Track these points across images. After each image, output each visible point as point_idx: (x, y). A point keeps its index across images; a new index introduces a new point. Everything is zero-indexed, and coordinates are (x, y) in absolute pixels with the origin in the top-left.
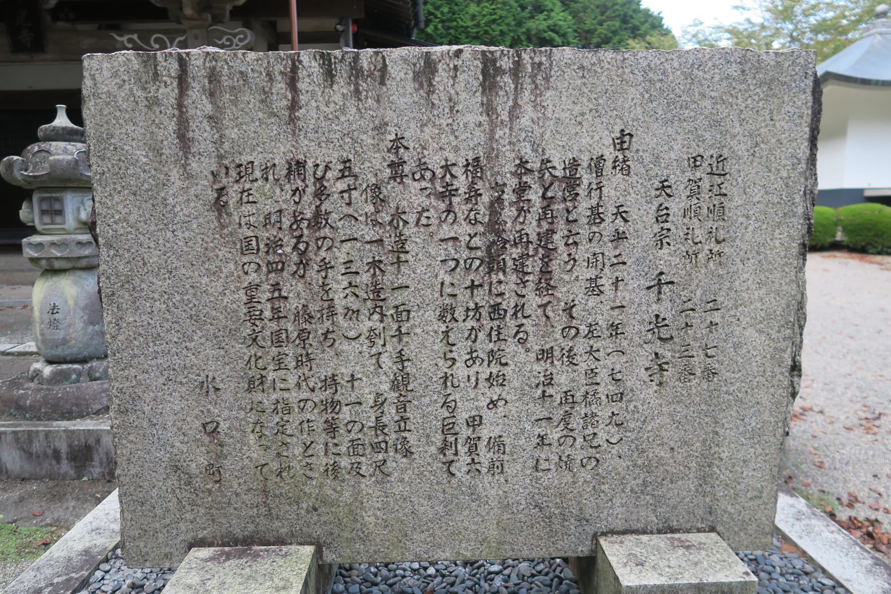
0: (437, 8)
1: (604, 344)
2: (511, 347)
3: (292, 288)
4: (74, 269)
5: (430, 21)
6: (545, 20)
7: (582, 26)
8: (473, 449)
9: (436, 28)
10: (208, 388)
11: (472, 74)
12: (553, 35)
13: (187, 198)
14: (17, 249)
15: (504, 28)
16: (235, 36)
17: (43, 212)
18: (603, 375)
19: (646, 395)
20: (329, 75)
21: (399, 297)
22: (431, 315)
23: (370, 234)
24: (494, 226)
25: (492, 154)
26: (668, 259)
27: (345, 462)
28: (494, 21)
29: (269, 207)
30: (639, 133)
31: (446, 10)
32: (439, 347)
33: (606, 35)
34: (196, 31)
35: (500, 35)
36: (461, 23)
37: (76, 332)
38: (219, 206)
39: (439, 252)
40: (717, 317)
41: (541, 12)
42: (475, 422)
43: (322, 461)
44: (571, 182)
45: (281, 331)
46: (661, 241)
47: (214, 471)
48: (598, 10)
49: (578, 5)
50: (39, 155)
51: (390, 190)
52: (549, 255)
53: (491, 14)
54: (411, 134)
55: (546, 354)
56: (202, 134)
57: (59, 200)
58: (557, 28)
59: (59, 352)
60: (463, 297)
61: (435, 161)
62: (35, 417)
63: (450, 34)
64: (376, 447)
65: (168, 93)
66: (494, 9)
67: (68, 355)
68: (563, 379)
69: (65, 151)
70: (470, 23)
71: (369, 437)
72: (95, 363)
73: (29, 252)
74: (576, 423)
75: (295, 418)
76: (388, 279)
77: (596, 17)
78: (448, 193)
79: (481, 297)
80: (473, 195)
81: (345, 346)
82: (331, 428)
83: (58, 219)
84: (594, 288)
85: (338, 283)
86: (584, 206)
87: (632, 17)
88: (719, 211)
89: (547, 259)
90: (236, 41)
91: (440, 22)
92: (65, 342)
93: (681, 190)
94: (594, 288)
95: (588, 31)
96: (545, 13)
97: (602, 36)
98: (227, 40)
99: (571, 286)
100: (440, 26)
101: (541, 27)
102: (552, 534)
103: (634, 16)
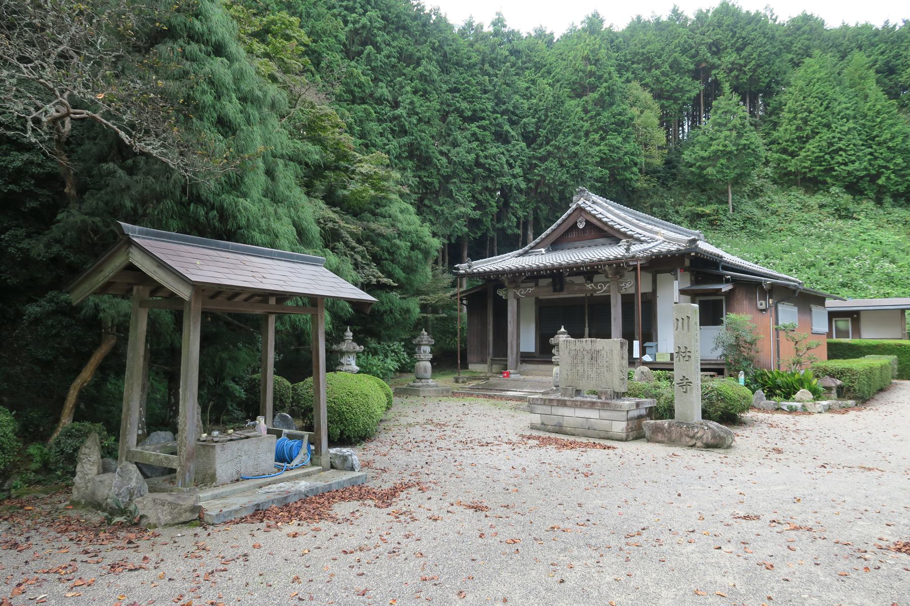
5: (883, 173)
9: (888, 178)
13: (567, 352)
91: (893, 173)
99: (599, 362)
100: (892, 176)
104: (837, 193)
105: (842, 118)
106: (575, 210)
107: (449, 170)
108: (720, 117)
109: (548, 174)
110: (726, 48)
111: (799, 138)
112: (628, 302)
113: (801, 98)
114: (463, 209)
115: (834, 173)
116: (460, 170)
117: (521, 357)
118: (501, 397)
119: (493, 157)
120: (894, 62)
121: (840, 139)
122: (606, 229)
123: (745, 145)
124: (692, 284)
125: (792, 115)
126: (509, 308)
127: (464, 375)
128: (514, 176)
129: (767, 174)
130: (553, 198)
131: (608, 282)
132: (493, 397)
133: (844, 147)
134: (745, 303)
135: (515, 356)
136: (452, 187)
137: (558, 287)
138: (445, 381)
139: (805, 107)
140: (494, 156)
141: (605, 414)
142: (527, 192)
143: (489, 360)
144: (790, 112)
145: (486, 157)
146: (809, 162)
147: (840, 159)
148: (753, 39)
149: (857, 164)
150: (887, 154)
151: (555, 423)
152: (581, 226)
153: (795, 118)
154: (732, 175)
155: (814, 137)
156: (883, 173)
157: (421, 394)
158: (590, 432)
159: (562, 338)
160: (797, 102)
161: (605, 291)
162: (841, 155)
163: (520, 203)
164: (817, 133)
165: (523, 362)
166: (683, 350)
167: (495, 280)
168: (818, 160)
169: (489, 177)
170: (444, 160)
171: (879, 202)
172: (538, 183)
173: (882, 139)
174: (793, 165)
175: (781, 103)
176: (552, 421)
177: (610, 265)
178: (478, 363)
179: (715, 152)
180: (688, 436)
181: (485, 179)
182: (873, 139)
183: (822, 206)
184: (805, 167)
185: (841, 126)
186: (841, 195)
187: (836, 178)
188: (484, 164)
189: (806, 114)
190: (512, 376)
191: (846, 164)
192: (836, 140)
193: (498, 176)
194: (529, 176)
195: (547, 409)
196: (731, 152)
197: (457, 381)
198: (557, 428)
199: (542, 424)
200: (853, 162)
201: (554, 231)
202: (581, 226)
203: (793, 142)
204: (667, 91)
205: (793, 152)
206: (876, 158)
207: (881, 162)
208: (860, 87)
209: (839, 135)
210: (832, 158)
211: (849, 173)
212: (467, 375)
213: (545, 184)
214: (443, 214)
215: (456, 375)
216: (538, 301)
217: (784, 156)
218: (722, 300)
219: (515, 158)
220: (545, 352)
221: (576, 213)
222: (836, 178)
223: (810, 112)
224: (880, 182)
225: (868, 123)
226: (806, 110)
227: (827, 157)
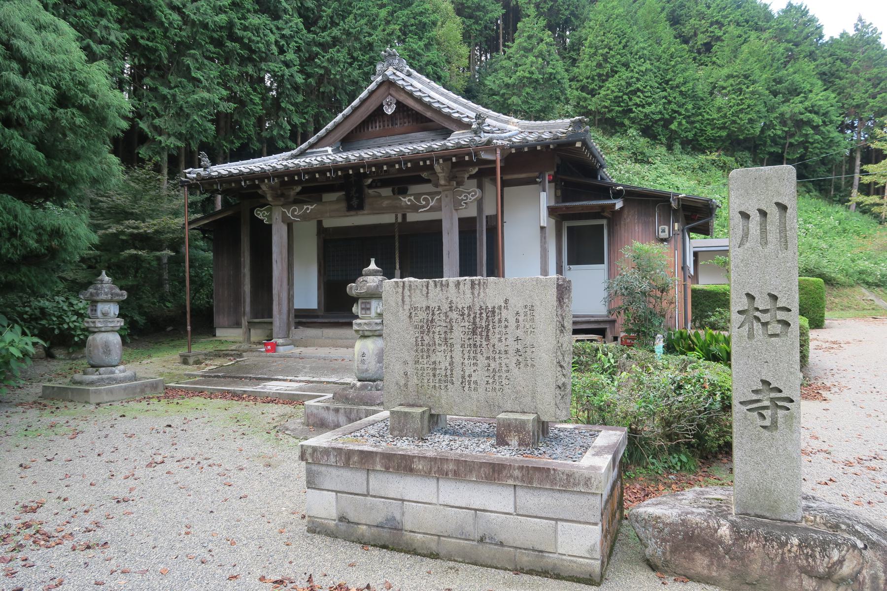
0: (681, 106)
1: (503, 356)
2: (479, 355)
3: (426, 338)
4: (373, 336)
5: (675, 118)
6: (801, 102)
7: (850, 101)
8: (469, 384)
9: (680, 124)
10: (406, 363)
11: (469, 285)
12: (812, 116)
13: (403, 315)
14: (350, 324)
15: (753, 115)
16: (469, 193)
17: (362, 309)
18: (503, 364)
19: (515, 371)
20: (436, 285)
21: (451, 341)
22: (459, 346)
23: (445, 325)
24: (474, 323)
25: (474, 305)
26: (520, 333)
27: (437, 385)
28: (741, 110)
29: (421, 317)
30: (510, 299)
31: (690, 106)
32: (461, 355)
35: (749, 123)
36: (706, 116)
37: (372, 366)
38: (410, 317)
39: (461, 329)
40: (534, 349)
41: (798, 95)
42: (470, 376)
43: (432, 384)
44: (493, 312)
45: (423, 349)
46: (517, 327)
47: (406, 385)
48: (869, 84)
49: (845, 81)
51: (449, 313)
52: (488, 331)
53: (738, 105)
54: (454, 300)
55: (488, 358)
56: (407, 299)
57: (369, 303)
58: (816, 109)
59: (364, 375)
60: (467, 341)
61: (460, 307)
63: (695, 127)
64: (445, 381)
65: (400, 290)
66: (741, 100)
68: (493, 365)
69: (373, 281)
70: (715, 116)
71: (443, 378)
72: (379, 382)
73: (355, 327)
74: (496, 378)
75: (426, 372)
76: (448, 336)
77: (867, 91)
78: (463, 315)
79: (471, 342)
80: (469, 315)
81: (438, 353)
82: (434, 375)
83: (368, 312)
84: (500, 340)
85: (437, 337)
86: (497, 318)
88: (533, 320)
89: (488, 332)
90: (470, 196)
91: (684, 118)
92: (367, 370)
93: (522, 314)
94: (500, 340)
95: (858, 106)
96: (802, 95)
99: (494, 340)
100: (684, 122)
101: (796, 110)
102: (491, 410)
104: (634, 136)
105: (640, 58)
106: (380, 85)
107: (183, 33)
108: (526, 41)
111: (600, 75)
112: (467, 228)
113: (602, 33)
114: (206, 95)
115: (632, 115)
116: (202, 39)
117: (296, 316)
118: (255, 397)
119: (257, 30)
120: (679, 12)
121: (638, 80)
122: (429, 114)
123: (551, 74)
124: (557, 202)
125: (593, 51)
126: (275, 239)
127: (202, 347)
128: (287, 64)
129: (567, 112)
131: (438, 193)
132: (237, 396)
133: (641, 88)
134: (638, 229)
135: (285, 317)
136: (188, 61)
137: (355, 202)
138: (160, 364)
139: (605, 43)
140: (257, 29)
141: (531, 500)
142: (308, 91)
143: (244, 322)
144: (590, 47)
145: (245, 28)
146: (609, 102)
147: (638, 101)
149: (653, 106)
150: (679, 99)
151: (379, 518)
152: (389, 111)
153: (595, 54)
154: (538, 107)
155: (613, 76)
156: (675, 118)
157: (93, 399)
158: (486, 551)
159: (371, 278)
160: (597, 36)
161: (432, 209)
162: (639, 97)
163: (295, 105)
164: (616, 72)
165: (298, 324)
166: (762, 303)
167: (247, 191)
168: (617, 101)
169: (250, 59)
170: (175, 17)
171: (670, 148)
172: (321, 79)
173: (675, 83)
174: (593, 104)
175: (581, 37)
176: (369, 515)
177: (447, 159)
178: (230, 327)
179: (521, 79)
180: (810, 573)
181: (243, 61)
182: (667, 82)
183: (621, 149)
184: (606, 107)
185: (639, 65)
186: (638, 138)
187: (633, 121)
188: (242, 38)
189: (606, 50)
190: (281, 350)
191: (643, 107)
192: (634, 80)
193: (263, 60)
194: (309, 69)
195: (354, 479)
196: (537, 81)
197: (185, 361)
198: (385, 534)
199: (342, 519)
200: (650, 104)
201: (346, 118)
202: (389, 111)
203: (593, 79)
204: (468, 7)
205: (593, 90)
206: (670, 102)
207: (674, 106)
208: (653, 30)
209: (636, 75)
210: (631, 99)
211: (646, 116)
212: (210, 348)
213: (330, 82)
214: (175, 101)
215: (184, 351)
216: (322, 231)
217: (584, 94)
219: (288, 38)
220: (337, 307)
221: (383, 89)
222: (633, 121)
223: (610, 49)
224: (674, 126)
225: (663, 66)
226: (606, 46)
227: (625, 97)
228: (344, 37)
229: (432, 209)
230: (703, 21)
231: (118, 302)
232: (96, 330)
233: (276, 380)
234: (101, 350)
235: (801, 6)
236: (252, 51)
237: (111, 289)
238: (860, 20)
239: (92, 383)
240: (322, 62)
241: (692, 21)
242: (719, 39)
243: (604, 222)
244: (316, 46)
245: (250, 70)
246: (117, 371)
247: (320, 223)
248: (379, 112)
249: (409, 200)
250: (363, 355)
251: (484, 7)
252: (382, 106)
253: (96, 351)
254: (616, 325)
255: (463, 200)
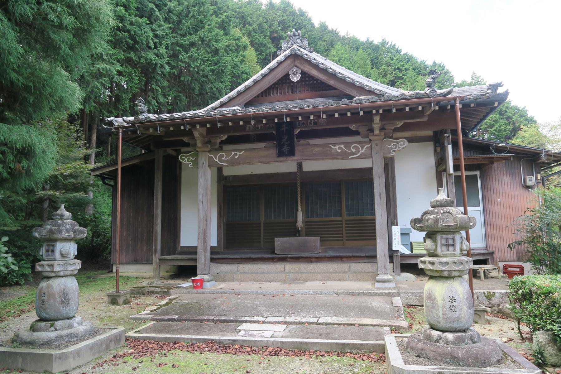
33: (490, 123)
34: (377, 142)
50: (444, 214)
57: (53, 246)
62: (466, 364)
67: (458, 327)
87: (506, 111)
92: (459, 319)
97: (488, 124)
98: (393, 145)
103: (507, 111)
106: (287, 58)
109: (193, 61)
110: (289, 27)
122: (332, 82)
130: (193, 89)
137: (286, 149)
148: (305, 26)
152: (295, 79)
163: (163, 88)
190: (207, 285)
197: (114, 300)
218: (476, 176)
221: (289, 62)
228: (200, 42)
229: (362, 157)
230: (390, 68)
231: (77, 242)
232: (53, 275)
233: (246, 322)
234: (58, 299)
235: (440, 64)
236: (136, 42)
237: (73, 226)
238: (474, 73)
239: (48, 344)
240: (185, 59)
241: (383, 66)
242: (399, 78)
243: (477, 173)
244: (179, 46)
245: (133, 55)
246: (75, 325)
247: (220, 170)
248: (285, 79)
249: (339, 148)
250: (453, 300)
251: (265, 45)
252: (287, 75)
253: (52, 301)
254: (494, 256)
255: (392, 148)
